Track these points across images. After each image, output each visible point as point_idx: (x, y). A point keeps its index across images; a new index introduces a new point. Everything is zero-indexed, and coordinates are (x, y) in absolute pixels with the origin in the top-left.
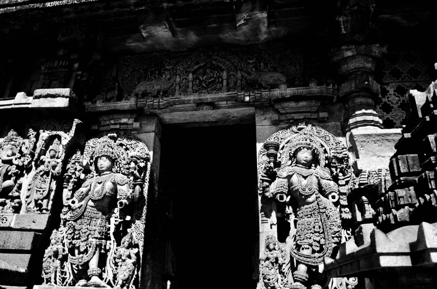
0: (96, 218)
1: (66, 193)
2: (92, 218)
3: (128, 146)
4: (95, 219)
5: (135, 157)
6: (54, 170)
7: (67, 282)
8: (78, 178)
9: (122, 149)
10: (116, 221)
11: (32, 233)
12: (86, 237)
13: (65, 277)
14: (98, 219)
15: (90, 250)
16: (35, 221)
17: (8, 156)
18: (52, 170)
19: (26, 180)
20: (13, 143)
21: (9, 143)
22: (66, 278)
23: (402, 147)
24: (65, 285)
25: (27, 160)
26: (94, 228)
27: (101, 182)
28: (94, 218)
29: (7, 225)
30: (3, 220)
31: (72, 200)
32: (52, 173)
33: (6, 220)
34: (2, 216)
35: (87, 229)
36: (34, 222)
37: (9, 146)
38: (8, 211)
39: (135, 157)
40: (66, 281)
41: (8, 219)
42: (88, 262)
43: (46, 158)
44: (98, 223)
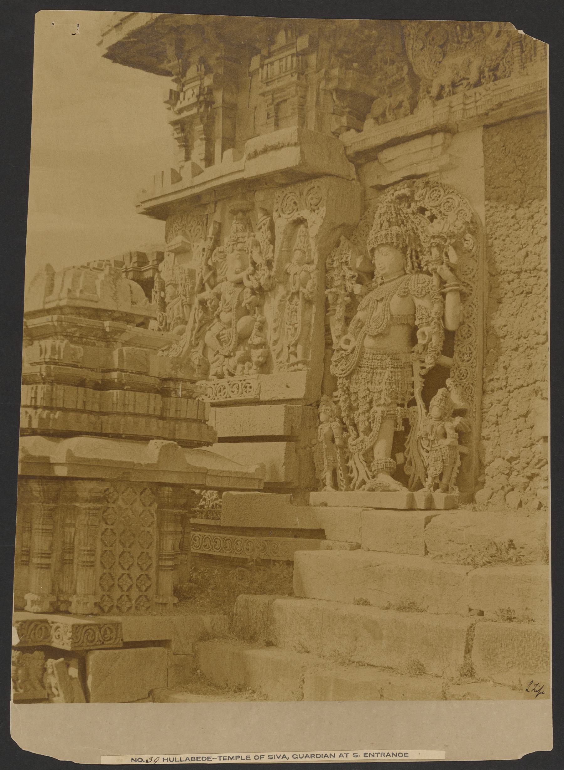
0: (382, 369)
1: (336, 327)
2: (374, 369)
3: (435, 211)
4: (379, 371)
5: (439, 237)
6: (305, 287)
7: (355, 484)
8: (352, 295)
9: (424, 219)
10: (423, 368)
11: (280, 409)
12: (367, 406)
13: (352, 475)
14: (385, 369)
15: (376, 427)
16: (289, 385)
17: (237, 273)
18: (301, 289)
19: (270, 310)
20: (240, 246)
21: (235, 247)
22: (353, 478)
23: (492, 318)
24: (353, 490)
25: (264, 275)
26: (378, 387)
27: (382, 299)
28: (377, 368)
29: (251, 396)
30: (246, 387)
31: (344, 338)
32: (303, 294)
33: (251, 387)
34: (244, 380)
35: (369, 390)
36: (287, 387)
37: (236, 252)
38: (251, 371)
39: (439, 237)
40: (353, 482)
41: (252, 385)
42: (372, 449)
43: (292, 268)
44: (386, 377)
